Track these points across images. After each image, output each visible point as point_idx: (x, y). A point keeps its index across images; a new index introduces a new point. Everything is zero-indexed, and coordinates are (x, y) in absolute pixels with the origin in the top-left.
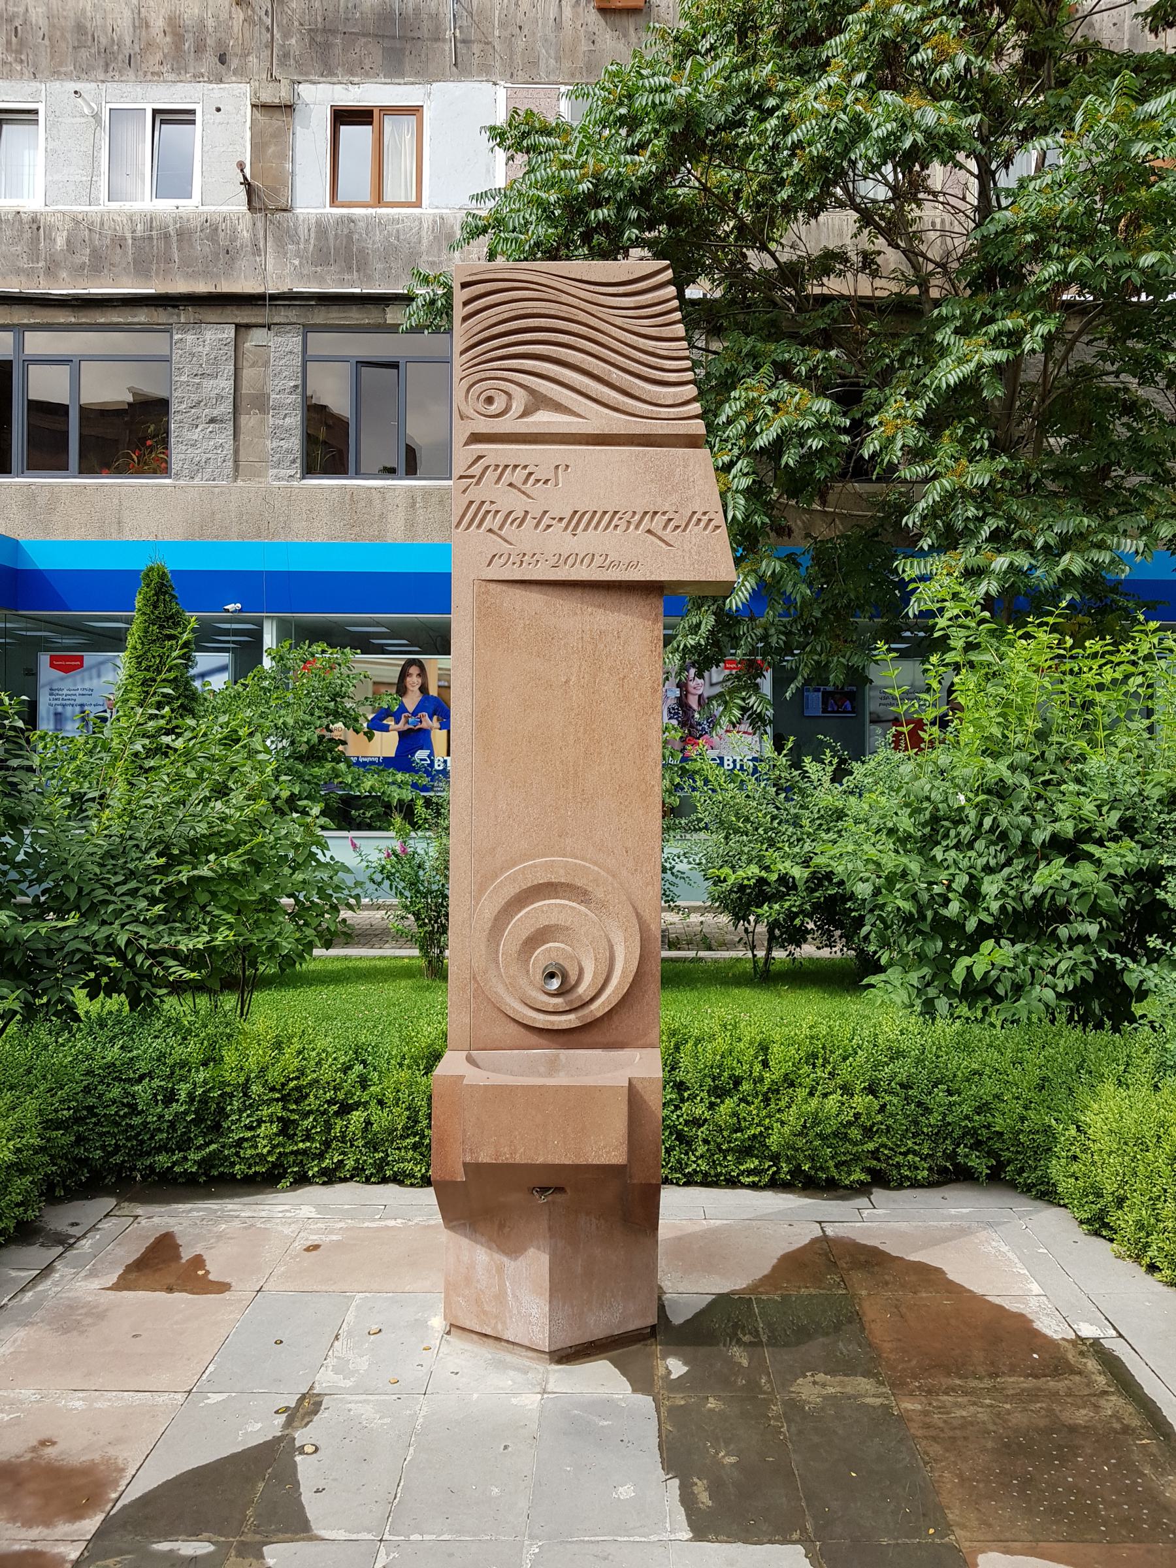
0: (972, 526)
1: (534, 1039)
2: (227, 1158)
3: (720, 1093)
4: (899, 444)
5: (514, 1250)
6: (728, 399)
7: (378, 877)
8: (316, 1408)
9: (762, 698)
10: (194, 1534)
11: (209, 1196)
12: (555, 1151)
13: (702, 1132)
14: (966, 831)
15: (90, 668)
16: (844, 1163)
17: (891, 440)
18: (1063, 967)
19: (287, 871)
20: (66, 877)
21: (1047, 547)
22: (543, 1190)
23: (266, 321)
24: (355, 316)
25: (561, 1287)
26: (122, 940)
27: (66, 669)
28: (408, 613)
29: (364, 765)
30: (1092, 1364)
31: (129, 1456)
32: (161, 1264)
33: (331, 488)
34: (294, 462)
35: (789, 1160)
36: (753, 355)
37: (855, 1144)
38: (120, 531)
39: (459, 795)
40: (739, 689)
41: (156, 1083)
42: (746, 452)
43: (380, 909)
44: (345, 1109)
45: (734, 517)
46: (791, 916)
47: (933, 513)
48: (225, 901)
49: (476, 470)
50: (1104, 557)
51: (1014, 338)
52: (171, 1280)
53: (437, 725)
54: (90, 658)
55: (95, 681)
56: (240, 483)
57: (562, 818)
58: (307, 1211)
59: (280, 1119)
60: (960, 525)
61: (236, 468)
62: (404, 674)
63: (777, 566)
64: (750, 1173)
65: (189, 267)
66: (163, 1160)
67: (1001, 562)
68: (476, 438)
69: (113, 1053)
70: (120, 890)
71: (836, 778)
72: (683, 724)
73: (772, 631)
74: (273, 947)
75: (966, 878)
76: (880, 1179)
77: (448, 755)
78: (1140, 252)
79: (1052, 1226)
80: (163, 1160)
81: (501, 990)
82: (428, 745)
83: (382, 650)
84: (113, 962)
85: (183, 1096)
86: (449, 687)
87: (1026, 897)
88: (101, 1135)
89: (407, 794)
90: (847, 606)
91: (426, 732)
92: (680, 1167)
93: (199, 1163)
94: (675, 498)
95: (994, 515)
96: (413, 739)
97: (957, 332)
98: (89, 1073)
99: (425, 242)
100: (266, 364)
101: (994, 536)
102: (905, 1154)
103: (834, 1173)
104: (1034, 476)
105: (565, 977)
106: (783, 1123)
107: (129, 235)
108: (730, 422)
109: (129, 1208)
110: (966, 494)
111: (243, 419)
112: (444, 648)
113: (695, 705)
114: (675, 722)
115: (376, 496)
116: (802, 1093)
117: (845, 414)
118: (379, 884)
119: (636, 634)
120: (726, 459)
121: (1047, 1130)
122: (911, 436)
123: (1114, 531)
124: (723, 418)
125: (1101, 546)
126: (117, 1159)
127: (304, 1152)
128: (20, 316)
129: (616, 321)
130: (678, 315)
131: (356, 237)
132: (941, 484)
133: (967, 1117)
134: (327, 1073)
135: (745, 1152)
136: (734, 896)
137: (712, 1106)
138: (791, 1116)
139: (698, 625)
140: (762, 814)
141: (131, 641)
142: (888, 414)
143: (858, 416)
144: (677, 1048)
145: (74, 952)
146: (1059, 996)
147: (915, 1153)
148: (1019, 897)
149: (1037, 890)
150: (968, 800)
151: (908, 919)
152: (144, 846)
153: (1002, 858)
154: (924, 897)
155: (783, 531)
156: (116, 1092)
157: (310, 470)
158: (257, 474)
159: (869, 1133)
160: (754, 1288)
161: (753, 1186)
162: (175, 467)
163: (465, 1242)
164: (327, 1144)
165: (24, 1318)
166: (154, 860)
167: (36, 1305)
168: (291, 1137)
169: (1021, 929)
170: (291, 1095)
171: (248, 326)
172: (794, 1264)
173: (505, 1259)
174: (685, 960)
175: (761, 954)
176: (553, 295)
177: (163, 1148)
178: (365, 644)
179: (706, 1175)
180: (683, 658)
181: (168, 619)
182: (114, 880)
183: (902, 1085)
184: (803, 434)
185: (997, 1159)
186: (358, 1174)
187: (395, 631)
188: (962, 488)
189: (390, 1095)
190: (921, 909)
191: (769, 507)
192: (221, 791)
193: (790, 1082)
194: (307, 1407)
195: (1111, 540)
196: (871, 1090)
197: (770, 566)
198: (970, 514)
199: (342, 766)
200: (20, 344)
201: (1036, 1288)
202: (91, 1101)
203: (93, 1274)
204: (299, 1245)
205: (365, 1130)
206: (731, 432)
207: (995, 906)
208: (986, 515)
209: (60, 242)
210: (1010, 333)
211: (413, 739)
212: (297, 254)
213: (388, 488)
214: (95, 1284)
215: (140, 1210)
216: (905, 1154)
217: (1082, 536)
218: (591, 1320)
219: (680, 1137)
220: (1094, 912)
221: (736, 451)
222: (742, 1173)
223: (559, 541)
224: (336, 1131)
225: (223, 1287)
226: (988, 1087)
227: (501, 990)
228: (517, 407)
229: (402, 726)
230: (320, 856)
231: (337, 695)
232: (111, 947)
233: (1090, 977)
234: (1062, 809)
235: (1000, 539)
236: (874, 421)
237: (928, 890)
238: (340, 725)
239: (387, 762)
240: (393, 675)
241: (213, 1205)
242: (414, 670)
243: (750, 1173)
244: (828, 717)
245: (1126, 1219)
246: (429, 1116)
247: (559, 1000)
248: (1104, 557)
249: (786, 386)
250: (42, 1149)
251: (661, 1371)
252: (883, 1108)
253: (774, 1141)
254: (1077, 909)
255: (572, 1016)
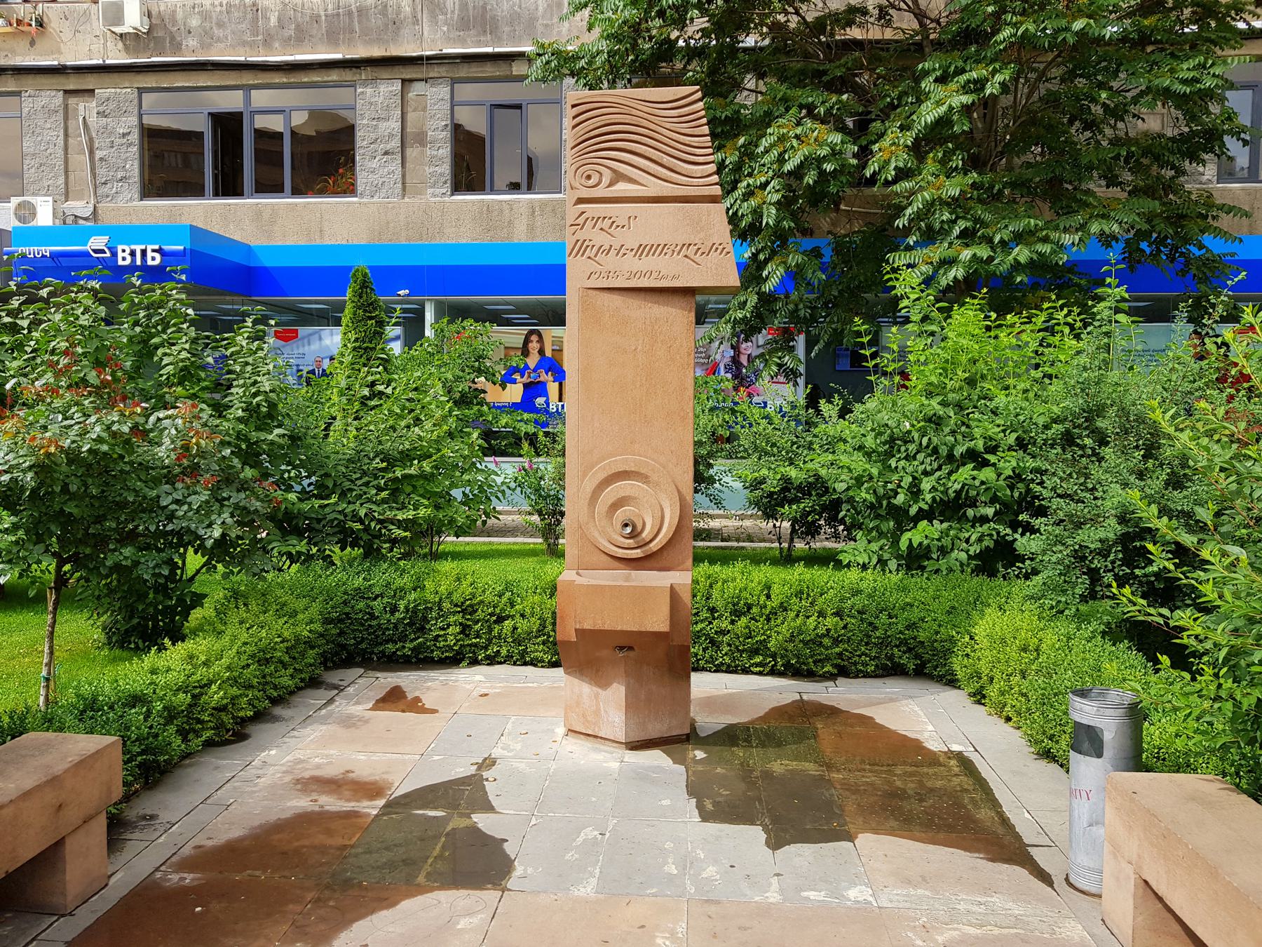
0: (946, 227)
1: (616, 564)
2: (428, 647)
3: (737, 613)
4: (893, 165)
5: (604, 685)
6: (764, 135)
7: (513, 485)
8: (494, 763)
9: (795, 358)
10: (435, 808)
11: (419, 669)
12: (628, 623)
13: (726, 638)
14: (912, 448)
15: (303, 338)
16: (820, 660)
17: (887, 162)
18: (973, 538)
19: (458, 474)
20: (327, 475)
21: (1002, 242)
22: (621, 648)
23: (424, 76)
24: (489, 70)
25: (632, 706)
26: (362, 513)
27: (286, 339)
28: (534, 296)
29: (501, 408)
30: (953, 762)
31: (395, 779)
32: (394, 699)
33: (473, 202)
34: (445, 183)
35: (782, 657)
36: (785, 100)
37: (827, 649)
38: (322, 237)
39: (572, 434)
40: (777, 350)
41: (386, 600)
42: (778, 175)
43: (514, 510)
44: (500, 620)
45: (767, 223)
46: (805, 514)
47: (919, 216)
48: (421, 491)
49: (581, 220)
50: (1046, 248)
51: (980, 84)
52: (402, 707)
53: (551, 379)
54: (303, 331)
55: (306, 348)
56: (406, 200)
57: (631, 424)
58: (478, 678)
59: (461, 624)
60: (937, 226)
61: (404, 189)
62: (527, 341)
63: (799, 258)
64: (757, 665)
65: (368, 36)
66: (390, 647)
67: (966, 254)
68: (581, 201)
69: (358, 582)
70: (359, 482)
71: (842, 415)
72: (735, 377)
73: (801, 306)
74: (452, 521)
75: (910, 479)
76: (843, 672)
77: (560, 400)
78: (1074, 19)
79: (955, 699)
80: (390, 647)
81: (596, 534)
82: (544, 393)
83: (509, 323)
84: (357, 526)
85: (402, 608)
86: (561, 350)
87: (950, 491)
88: (354, 631)
89: (531, 429)
90: (858, 287)
91: (543, 384)
92: (712, 660)
93: (412, 650)
94: (702, 235)
95: (964, 218)
96: (534, 389)
97: (936, 81)
98: (345, 593)
99: (540, 8)
100: (424, 109)
101: (964, 234)
102: (860, 656)
103: (812, 666)
104: (997, 187)
105: (634, 527)
106: (778, 633)
107: (322, 13)
108: (767, 151)
109: (371, 673)
110: (943, 203)
111: (409, 151)
112: (560, 321)
113: (745, 362)
114: (729, 376)
115: (506, 207)
116: (792, 614)
117: (854, 143)
118: (514, 490)
119: (678, 317)
120: (763, 179)
121: (951, 640)
122: (903, 159)
123: (1056, 228)
124: (761, 149)
125: (1045, 240)
126: (363, 646)
127: (475, 645)
128: (248, 78)
129: (667, 124)
130: (704, 120)
131: (489, 7)
132: (923, 197)
133: (901, 632)
134: (489, 597)
135: (754, 652)
136: (765, 500)
137: (732, 622)
138: (784, 629)
139: (745, 303)
140: (784, 441)
141: (344, 321)
142: (886, 142)
143: (864, 143)
144: (711, 586)
145: (332, 521)
146: (970, 557)
147: (866, 655)
148: (946, 492)
149: (957, 486)
150: (913, 426)
151: (872, 507)
152: (372, 455)
153: (935, 465)
154: (881, 491)
155: (807, 232)
156: (361, 605)
157: (457, 188)
158: (420, 193)
159: (836, 642)
160: (752, 722)
161: (760, 674)
162: (360, 189)
163: (576, 681)
164: (490, 641)
165: (324, 720)
166: (378, 464)
167: (330, 715)
168: (467, 636)
169: (948, 514)
170: (467, 609)
171: (411, 81)
172: (779, 713)
173: (600, 691)
174: (731, 548)
175: (785, 545)
176: (627, 110)
177: (390, 640)
178: (498, 318)
179: (729, 666)
180: (734, 327)
181: (369, 305)
182: (355, 476)
183: (859, 612)
184: (820, 160)
185: (923, 662)
186: (508, 660)
187: (519, 309)
188: (940, 198)
189: (528, 610)
190: (879, 500)
191: (794, 216)
192: (417, 421)
193: (784, 608)
194: (489, 763)
195: (1054, 235)
196: (838, 614)
197: (794, 259)
198: (944, 218)
199: (485, 408)
200: (248, 100)
201: (930, 728)
202: (347, 610)
203: (358, 703)
204: (475, 694)
205: (513, 632)
206: (766, 159)
207: (928, 497)
208: (957, 218)
209: (273, 21)
210: (975, 82)
211: (534, 389)
212: (446, 23)
213: (514, 201)
214: (360, 708)
215: (379, 675)
216: (860, 656)
217: (1031, 233)
218: (650, 727)
219: (713, 642)
220: (994, 500)
221: (771, 173)
222: (752, 665)
223: (633, 263)
224: (495, 632)
225: (434, 711)
226: (915, 614)
227: (596, 534)
228: (606, 181)
229: (525, 380)
230: (478, 465)
231: (480, 357)
232: (355, 517)
233: (992, 545)
234: (977, 432)
235: (967, 237)
236: (875, 147)
237: (884, 487)
238: (482, 379)
239: (515, 406)
240: (518, 341)
241: (423, 673)
242: (534, 338)
243: (757, 665)
244: (841, 373)
245: (992, 692)
246: (554, 624)
247: (631, 541)
248: (1046, 248)
249: (809, 123)
250: (321, 635)
251: (691, 756)
252: (845, 627)
253: (772, 644)
254: (983, 499)
255: (639, 551)
